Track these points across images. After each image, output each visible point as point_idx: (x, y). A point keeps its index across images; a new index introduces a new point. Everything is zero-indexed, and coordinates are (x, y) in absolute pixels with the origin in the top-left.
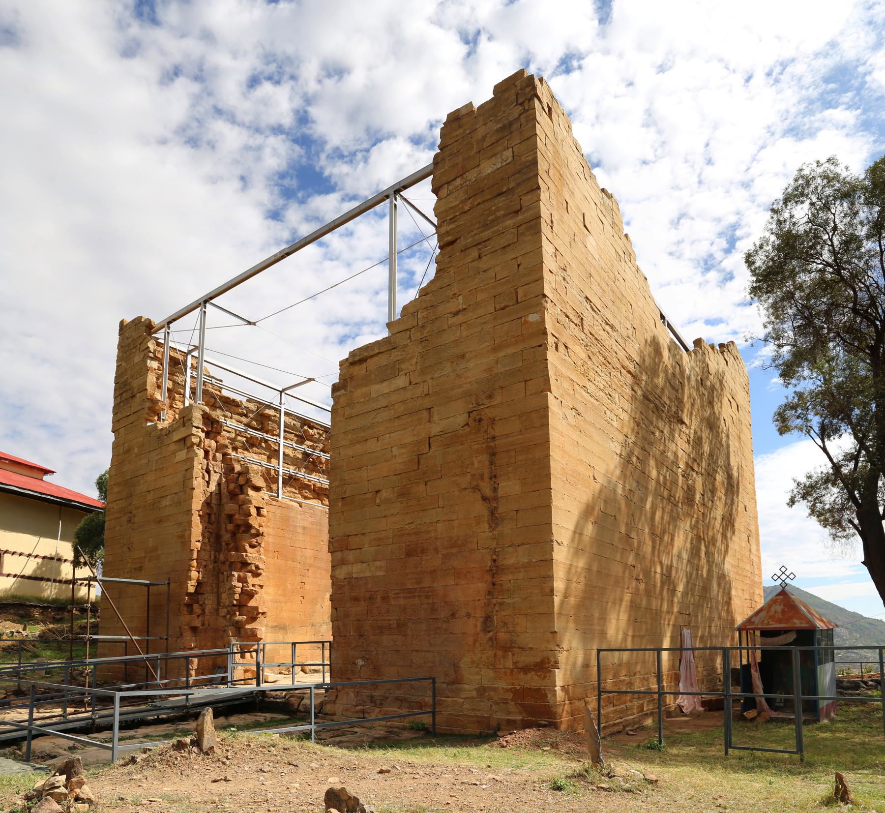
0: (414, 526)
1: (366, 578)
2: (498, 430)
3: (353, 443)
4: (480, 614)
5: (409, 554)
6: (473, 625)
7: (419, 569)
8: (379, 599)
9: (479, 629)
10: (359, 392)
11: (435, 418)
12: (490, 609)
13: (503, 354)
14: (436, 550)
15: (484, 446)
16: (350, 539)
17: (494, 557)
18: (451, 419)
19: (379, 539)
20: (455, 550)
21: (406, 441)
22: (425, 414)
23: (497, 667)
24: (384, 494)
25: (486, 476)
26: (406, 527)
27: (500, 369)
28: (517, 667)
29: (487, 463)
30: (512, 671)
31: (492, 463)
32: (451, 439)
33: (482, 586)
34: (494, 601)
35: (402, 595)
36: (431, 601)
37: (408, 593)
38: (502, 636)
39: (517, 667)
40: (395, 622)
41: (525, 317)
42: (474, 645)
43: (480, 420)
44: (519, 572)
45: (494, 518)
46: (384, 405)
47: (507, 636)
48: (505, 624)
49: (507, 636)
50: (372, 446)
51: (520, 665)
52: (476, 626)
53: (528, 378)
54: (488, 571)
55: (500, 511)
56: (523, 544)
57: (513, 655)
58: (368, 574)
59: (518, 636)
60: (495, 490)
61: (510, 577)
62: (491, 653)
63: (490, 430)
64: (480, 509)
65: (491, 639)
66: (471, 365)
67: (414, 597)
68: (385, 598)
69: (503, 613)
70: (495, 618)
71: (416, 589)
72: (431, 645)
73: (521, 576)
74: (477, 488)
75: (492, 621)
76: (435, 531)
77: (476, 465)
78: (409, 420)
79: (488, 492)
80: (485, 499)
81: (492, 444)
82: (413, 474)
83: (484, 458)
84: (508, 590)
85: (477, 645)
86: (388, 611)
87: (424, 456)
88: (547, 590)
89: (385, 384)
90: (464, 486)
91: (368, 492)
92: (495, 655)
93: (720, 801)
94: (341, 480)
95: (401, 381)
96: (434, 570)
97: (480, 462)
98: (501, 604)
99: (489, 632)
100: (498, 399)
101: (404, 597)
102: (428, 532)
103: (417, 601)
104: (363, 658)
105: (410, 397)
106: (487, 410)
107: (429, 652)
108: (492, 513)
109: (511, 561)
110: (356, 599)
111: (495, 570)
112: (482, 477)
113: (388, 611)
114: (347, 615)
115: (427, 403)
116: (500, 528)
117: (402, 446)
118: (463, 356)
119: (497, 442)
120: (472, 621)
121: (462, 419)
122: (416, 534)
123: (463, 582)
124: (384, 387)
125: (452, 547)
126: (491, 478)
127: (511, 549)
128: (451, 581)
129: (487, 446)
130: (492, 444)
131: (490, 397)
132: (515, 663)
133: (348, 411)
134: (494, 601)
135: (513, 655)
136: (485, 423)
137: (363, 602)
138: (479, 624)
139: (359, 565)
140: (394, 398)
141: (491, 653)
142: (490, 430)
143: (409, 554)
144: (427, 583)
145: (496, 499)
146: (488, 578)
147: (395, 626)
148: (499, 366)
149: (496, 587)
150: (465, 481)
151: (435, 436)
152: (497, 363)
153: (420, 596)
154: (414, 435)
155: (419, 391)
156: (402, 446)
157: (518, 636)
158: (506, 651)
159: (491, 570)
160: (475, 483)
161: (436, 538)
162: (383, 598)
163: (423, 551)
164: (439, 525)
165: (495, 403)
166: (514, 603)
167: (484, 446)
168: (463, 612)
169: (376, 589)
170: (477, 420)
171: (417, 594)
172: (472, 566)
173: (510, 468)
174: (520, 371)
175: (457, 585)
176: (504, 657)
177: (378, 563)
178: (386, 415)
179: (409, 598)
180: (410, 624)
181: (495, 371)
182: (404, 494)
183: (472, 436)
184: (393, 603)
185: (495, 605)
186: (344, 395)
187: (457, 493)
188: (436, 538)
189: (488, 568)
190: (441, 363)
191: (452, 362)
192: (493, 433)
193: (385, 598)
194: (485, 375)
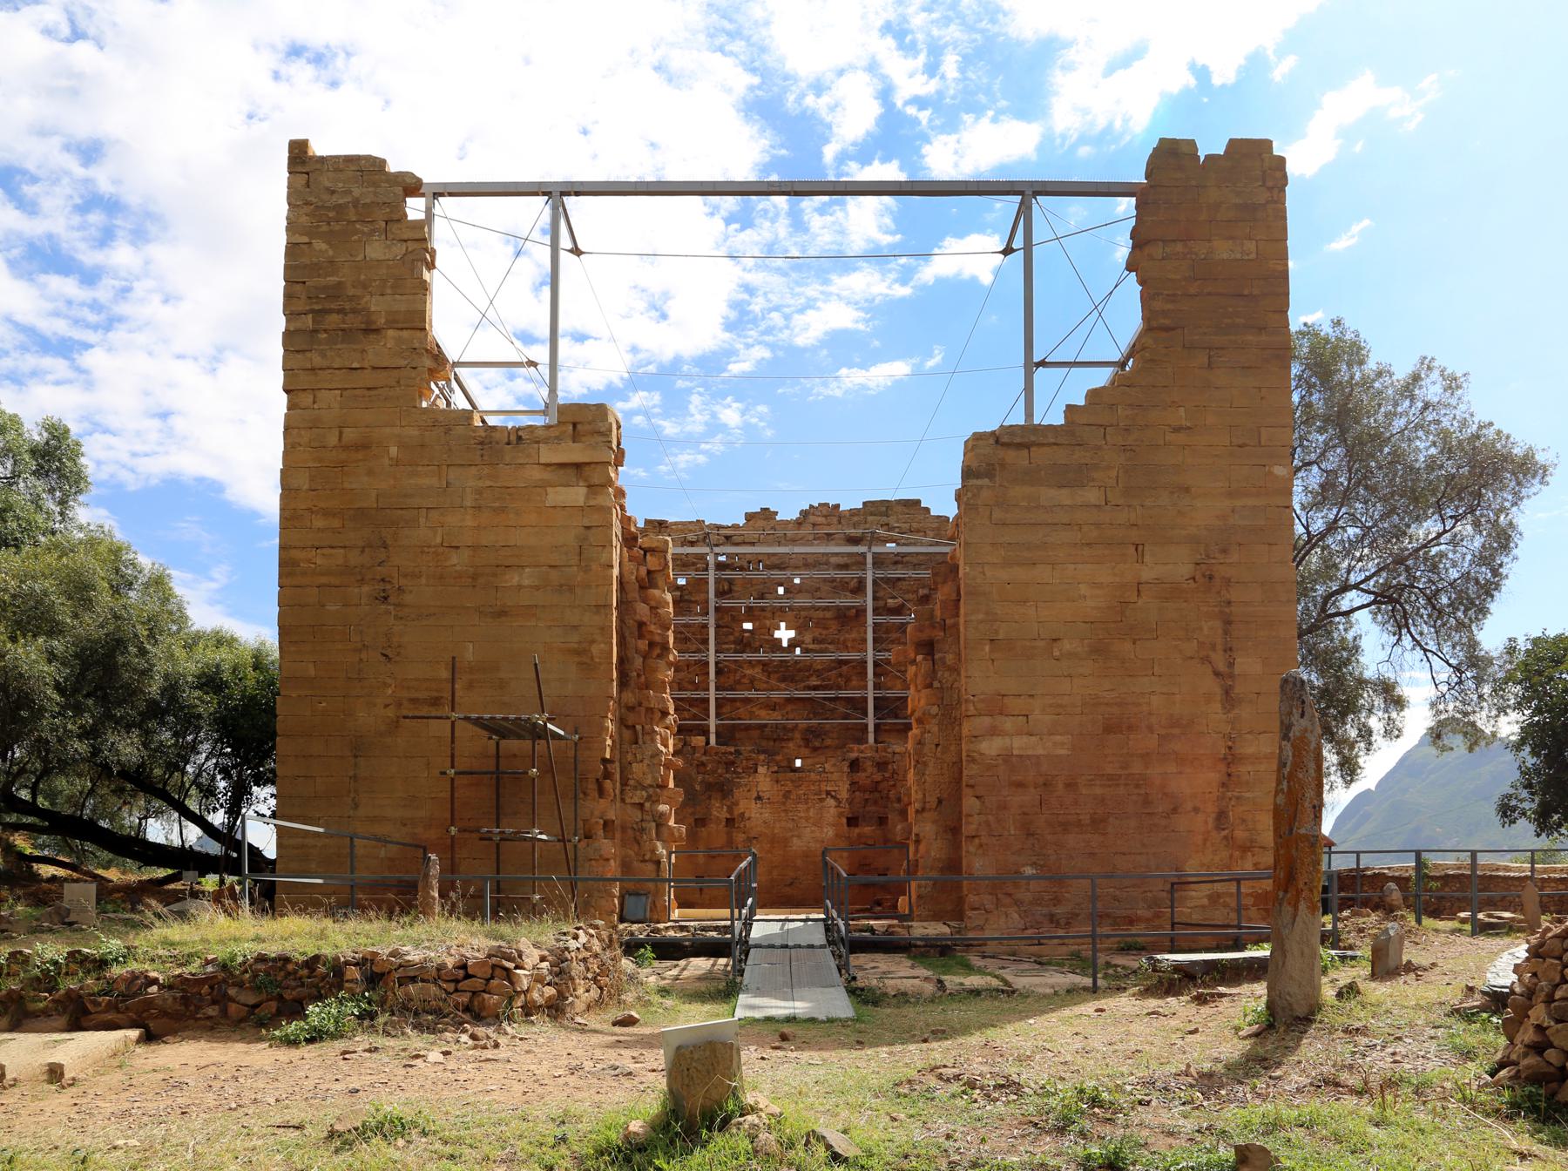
1: (1038, 757)
4: (1211, 809)
5: (1109, 729)
8: (1061, 786)
9: (1211, 825)
10: (1018, 492)
11: (1147, 558)
16: (1006, 700)
19: (1060, 706)
20: (1176, 731)
22: (1133, 549)
24: (1067, 646)
25: (1219, 647)
29: (1220, 631)
31: (1226, 632)
38: (1240, 834)
43: (1211, 577)
45: (1229, 699)
47: (1246, 834)
49: (1246, 834)
58: (1040, 752)
60: (1231, 665)
61: (1250, 768)
64: (1211, 685)
65: (1226, 838)
68: (1071, 786)
72: (1144, 845)
74: (1206, 660)
76: (1149, 704)
77: (1206, 631)
79: (1222, 667)
80: (1217, 674)
83: (1218, 624)
89: (1064, 491)
95: (1092, 496)
97: (1210, 629)
104: (1034, 864)
109: (1250, 750)
110: (1020, 785)
112: (1213, 647)
114: (1004, 807)
121: (1185, 570)
124: (1064, 496)
131: (1224, 551)
137: (1032, 790)
138: (1210, 820)
139: (1025, 739)
143: (1109, 729)
144: (1137, 768)
145: (1231, 676)
146: (1222, 767)
163: (1130, 728)
168: (1189, 806)
170: (1206, 578)
182: (1099, 650)
193: (1071, 786)
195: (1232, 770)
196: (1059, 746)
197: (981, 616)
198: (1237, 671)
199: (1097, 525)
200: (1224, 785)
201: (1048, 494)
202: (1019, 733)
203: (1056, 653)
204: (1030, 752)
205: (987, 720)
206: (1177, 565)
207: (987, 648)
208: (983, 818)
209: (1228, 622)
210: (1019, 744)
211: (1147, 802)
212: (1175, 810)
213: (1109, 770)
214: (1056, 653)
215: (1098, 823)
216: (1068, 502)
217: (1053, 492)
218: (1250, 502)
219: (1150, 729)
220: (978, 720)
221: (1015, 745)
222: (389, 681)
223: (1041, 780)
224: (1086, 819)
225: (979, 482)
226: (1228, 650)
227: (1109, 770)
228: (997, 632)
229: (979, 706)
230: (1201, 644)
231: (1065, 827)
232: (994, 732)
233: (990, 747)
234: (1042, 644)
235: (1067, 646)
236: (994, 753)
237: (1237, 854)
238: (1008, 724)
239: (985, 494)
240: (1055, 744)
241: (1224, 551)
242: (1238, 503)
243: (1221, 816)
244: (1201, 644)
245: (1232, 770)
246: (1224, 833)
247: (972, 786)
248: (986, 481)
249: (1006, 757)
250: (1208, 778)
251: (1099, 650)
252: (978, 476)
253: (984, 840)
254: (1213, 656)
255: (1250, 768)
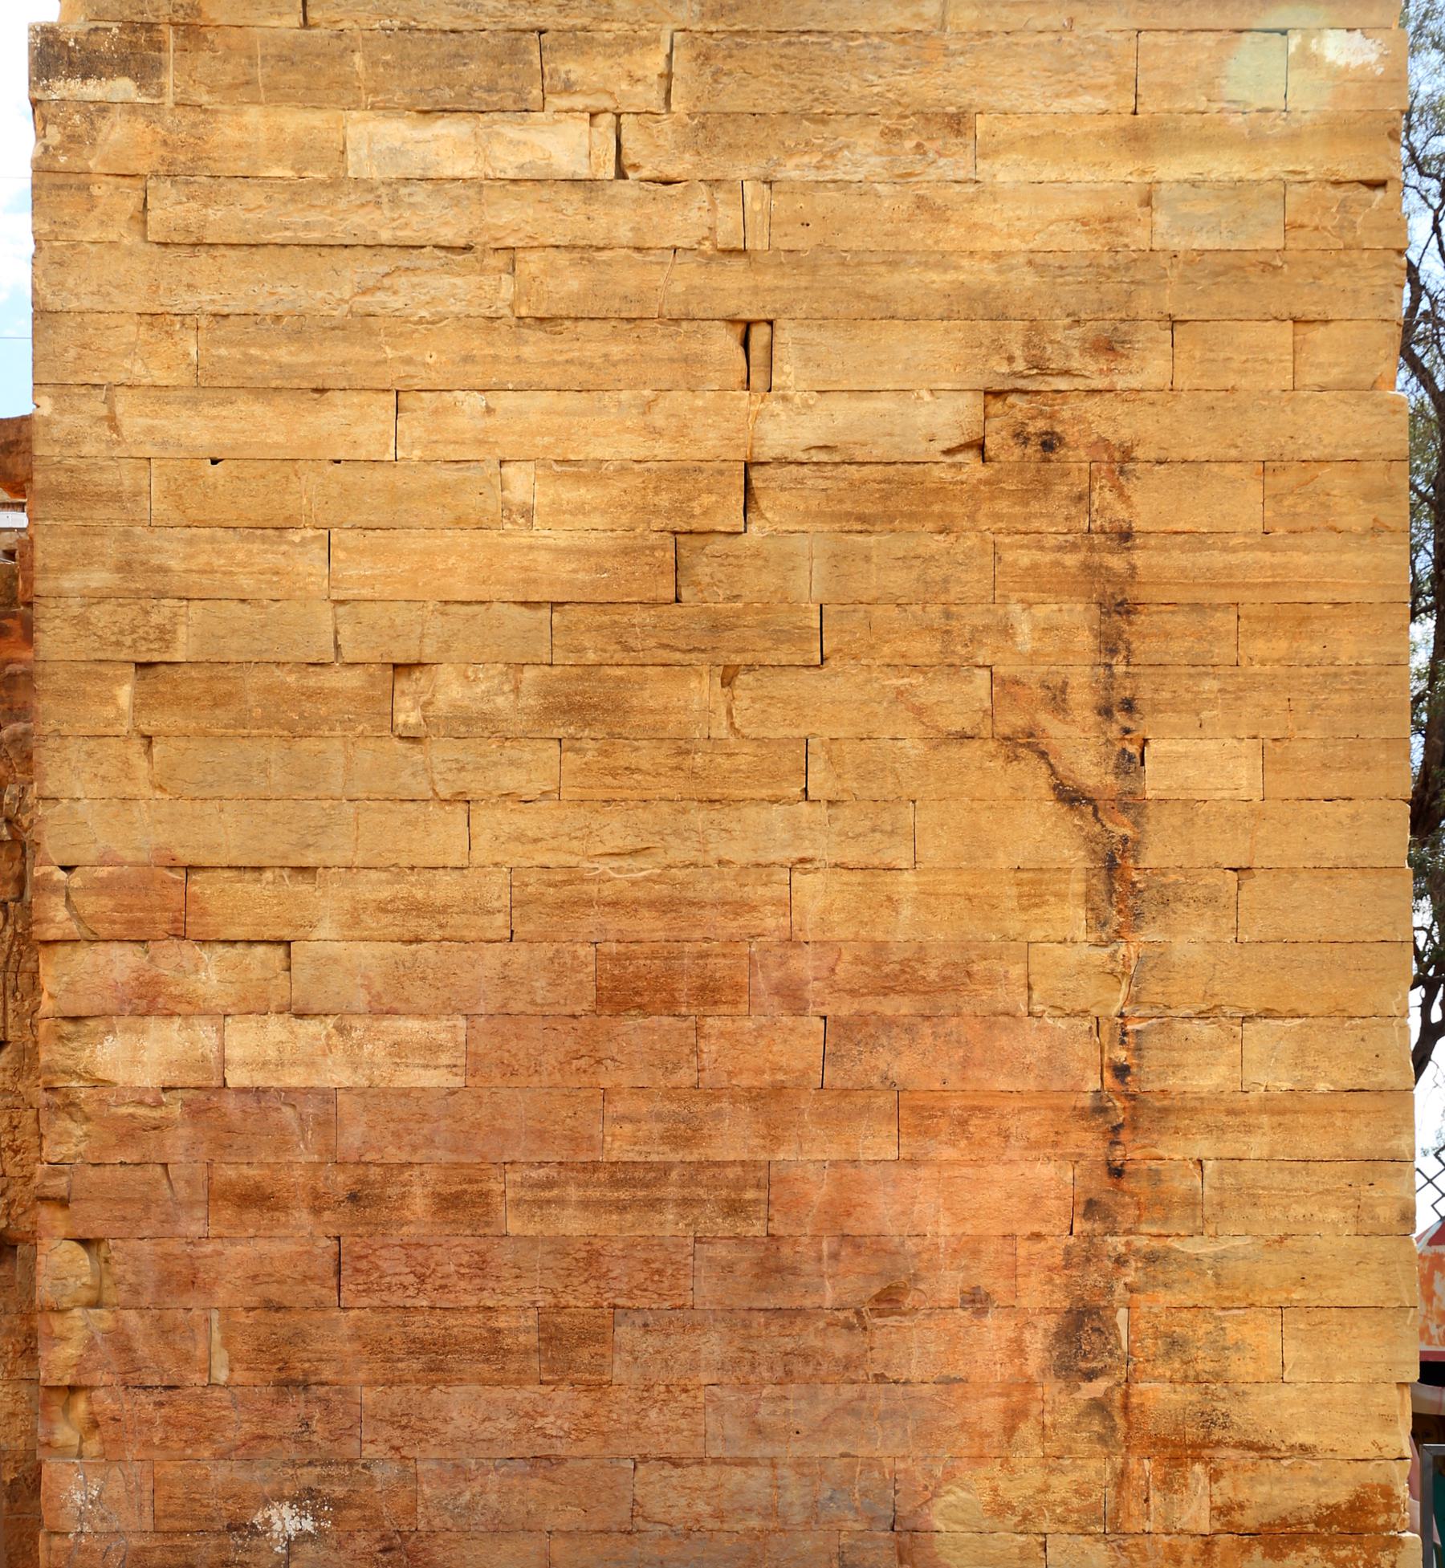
0: (645, 867)
1: (328, 1096)
2: (1145, 505)
3: (206, 386)
4: (1041, 1296)
5: (620, 995)
6: (1005, 1347)
7: (685, 1076)
8: (419, 1203)
9: (1034, 1362)
10: (250, 128)
11: (787, 373)
12: (1094, 1278)
13: (1184, 173)
14: (792, 996)
15: (1071, 560)
16: (200, 885)
17: (1121, 1055)
18: (884, 404)
19: (417, 909)
20: (901, 1006)
21: (598, 450)
22: (726, 341)
23: (1132, 1526)
24: (451, 689)
25: (1081, 697)
26: (605, 866)
27: (1164, 231)
28: (1232, 1529)
29: (1085, 640)
30: (1208, 1543)
31: (1110, 645)
32: (881, 494)
33: (1053, 1177)
34: (1117, 1244)
35: (573, 1193)
36: (758, 1229)
37: (616, 1184)
38: (1161, 1396)
39: (1232, 1529)
40: (530, 1320)
41: (1307, 34)
42: (1010, 1430)
43: (1050, 443)
44: (1248, 1129)
45: (1119, 885)
46: (447, 235)
47: (1187, 1395)
48: (1175, 1344)
49: (1187, 1395)
50: (358, 425)
51: (1249, 1519)
52: (1018, 1349)
53: (1312, 312)
54: (1082, 1114)
55: (1151, 858)
56: (1268, 1014)
57: (1215, 1476)
58: (336, 1075)
59: (1240, 1396)
60: (1130, 763)
61: (1203, 1147)
62: (1096, 1469)
63: (1103, 496)
64: (1055, 841)
65: (1099, 1407)
66: (1004, 172)
67: (654, 1204)
68: (461, 1203)
69: (1165, 1298)
70: (1122, 1316)
71: (666, 1168)
72: (759, 1431)
73: (1257, 1145)
74: (1025, 744)
75: (1106, 1329)
76: (787, 905)
77: (1025, 637)
78: (616, 350)
79: (1089, 769)
80: (1070, 796)
81: (1116, 562)
82: (641, 616)
83: (1077, 616)
84: (1192, 1202)
85: (1027, 1430)
86: (481, 1266)
87: (718, 545)
88: (1386, 1213)
89: (448, 129)
90: (958, 723)
91: (337, 659)
92: (1122, 1477)
93: (760, 563)
94: (125, 567)
95: (564, 144)
96: (778, 1090)
97: (1047, 632)
98: (1152, 1258)
99: (1090, 1376)
100: (1150, 367)
101: (585, 1204)
102: (741, 907)
103: (669, 1223)
104: (306, 1499)
105: (624, 234)
106: (1092, 405)
107: (744, 1463)
108: (1112, 864)
109: (1206, 1078)
110: (256, 1199)
111: (1124, 1107)
112: (1057, 698)
113: (481, 1266)
114: (185, 1279)
115: (735, 289)
116: (1152, 933)
117: (570, 469)
118: (958, 123)
119: (1139, 558)
120: (994, 1329)
121: (947, 415)
122: (665, 906)
123: (948, 1153)
124: (446, 146)
125: (886, 991)
126: (1106, 712)
127: (1206, 1031)
128: (878, 1143)
129: (1086, 567)
130: (1116, 562)
131: (1108, 347)
132: (1222, 1511)
133: (170, 209)
134: (1117, 1244)
135: (1215, 1476)
136: (1076, 457)
137: (302, 1216)
138: (1037, 1343)
139: (276, 1029)
140: (511, 217)
141: (1096, 1469)
142: (1103, 496)
143: (620, 995)
144: (733, 1140)
145: (1131, 804)
146: (1089, 1142)
147: (531, 1339)
148: (1161, 219)
149: (1127, 1184)
150: (963, 699)
151: (782, 462)
152: (1147, 202)
153: (686, 1203)
154: (655, 432)
155: (686, 220)
156: (570, 469)
157: (1240, 1396)
158: (1176, 1461)
159: (1101, 1110)
160: (1013, 720)
161: (791, 941)
162: (447, 1203)
163: (708, 993)
164: (807, 883)
165: (1135, 382)
166: (1218, 1258)
167: (1071, 560)
168: (949, 1284)
169: (394, 1155)
170: (1029, 441)
171: (672, 1192)
172: (1002, 1083)
173: (1209, 685)
174: (1268, 268)
175: (913, 1162)
176: (1166, 1485)
177: (411, 1027)
178: (455, 290)
179: (621, 1207)
180: (625, 1333)
181: (1138, 237)
182: (581, 708)
183: (1003, 506)
184: (514, 1226)
185: (1121, 1261)
186: (132, 108)
187: (913, 748)
188: (791, 941)
189: (1087, 1101)
190: (822, 120)
191: (893, 134)
192: (1121, 513)
193: (461, 1203)
194: (1083, 242)
195: (1131, 1151)
196: (417, 1057)
197: (100, 578)
198: (1154, 782)
199: (583, 251)
200: (1092, 1208)
201: (380, 140)
202: (254, 1007)
203: (408, 715)
204: (294, 1079)
205: (122, 961)
206: (923, 404)
207: (125, 694)
208: (103, 1319)
209: (1118, 607)
210: (252, 1049)
211: (772, 1267)
212: (889, 1300)
213: (619, 1147)
214: (408, 715)
215: (567, 1345)
216: (464, 167)
217: (396, 131)
218: (1225, 166)
219: (792, 996)
220: (85, 958)
221: (234, 1052)
222: (1118, 748)
223: (342, 1181)
224: (520, 1329)
225: (93, 90)
226: (1117, 707)
227: (619, 1146)
228: (165, 635)
229: (90, 905)
230: (1005, 687)
231: (437, 1359)
232: (149, 1001)
233: (133, 1059)
234: (352, 680)
235: (451, 689)
236: (148, 1078)
237: (1146, 1468)
238: (211, 973)
239: (116, 132)
240: (399, 1050)
241: (1108, 347)
242: (1170, 169)
243: (1081, 1330)
244: (1005, 687)
245: (1131, 1151)
246: (1098, 1388)
247: (63, 1203)
248: (122, 88)
249: (204, 1097)
250: (1025, 1184)
251: (581, 708)
252: (88, 65)
253: (106, 1402)
254: (1054, 728)
255: (1203, 1147)
